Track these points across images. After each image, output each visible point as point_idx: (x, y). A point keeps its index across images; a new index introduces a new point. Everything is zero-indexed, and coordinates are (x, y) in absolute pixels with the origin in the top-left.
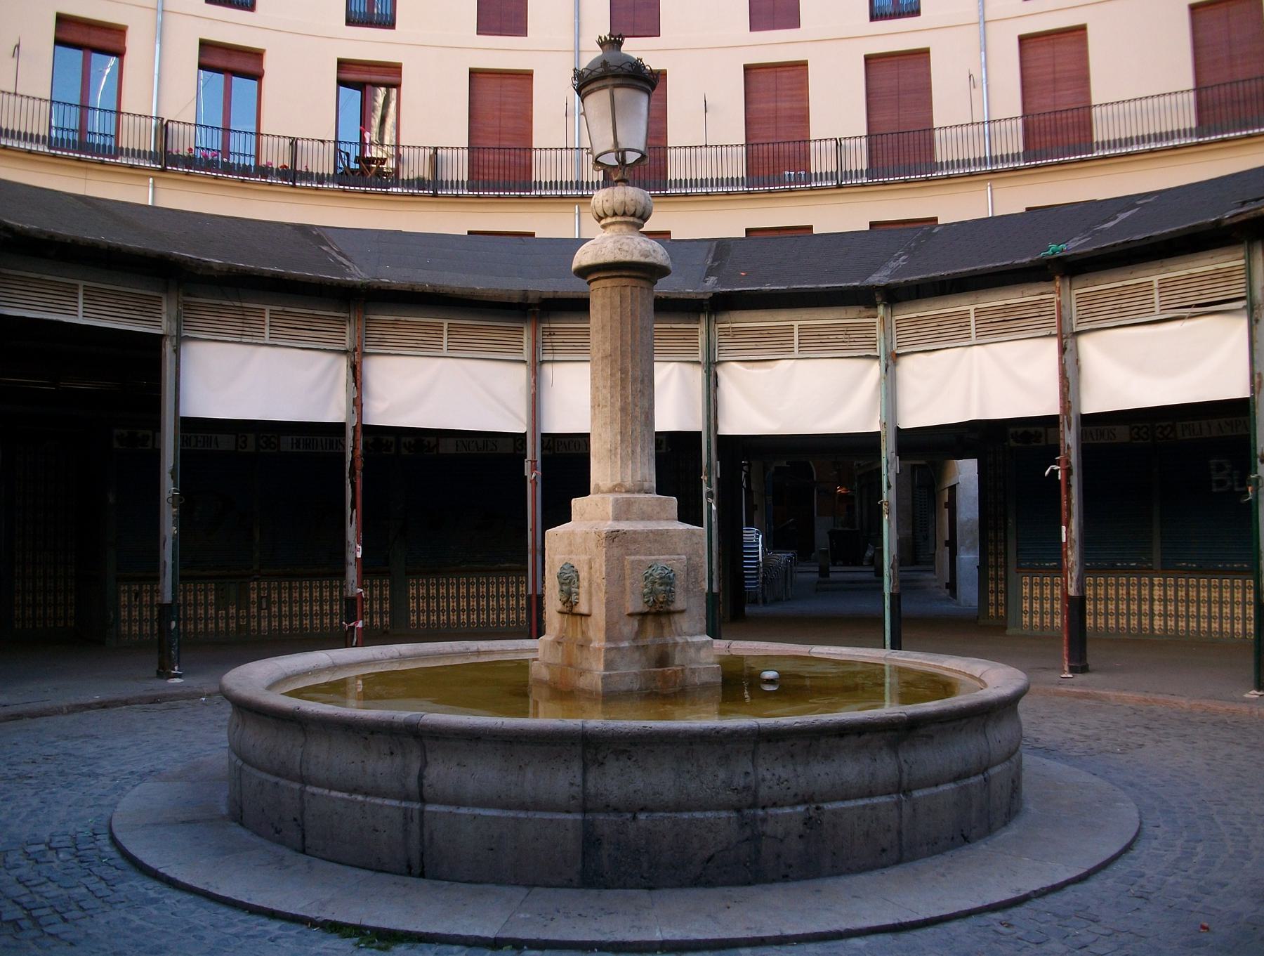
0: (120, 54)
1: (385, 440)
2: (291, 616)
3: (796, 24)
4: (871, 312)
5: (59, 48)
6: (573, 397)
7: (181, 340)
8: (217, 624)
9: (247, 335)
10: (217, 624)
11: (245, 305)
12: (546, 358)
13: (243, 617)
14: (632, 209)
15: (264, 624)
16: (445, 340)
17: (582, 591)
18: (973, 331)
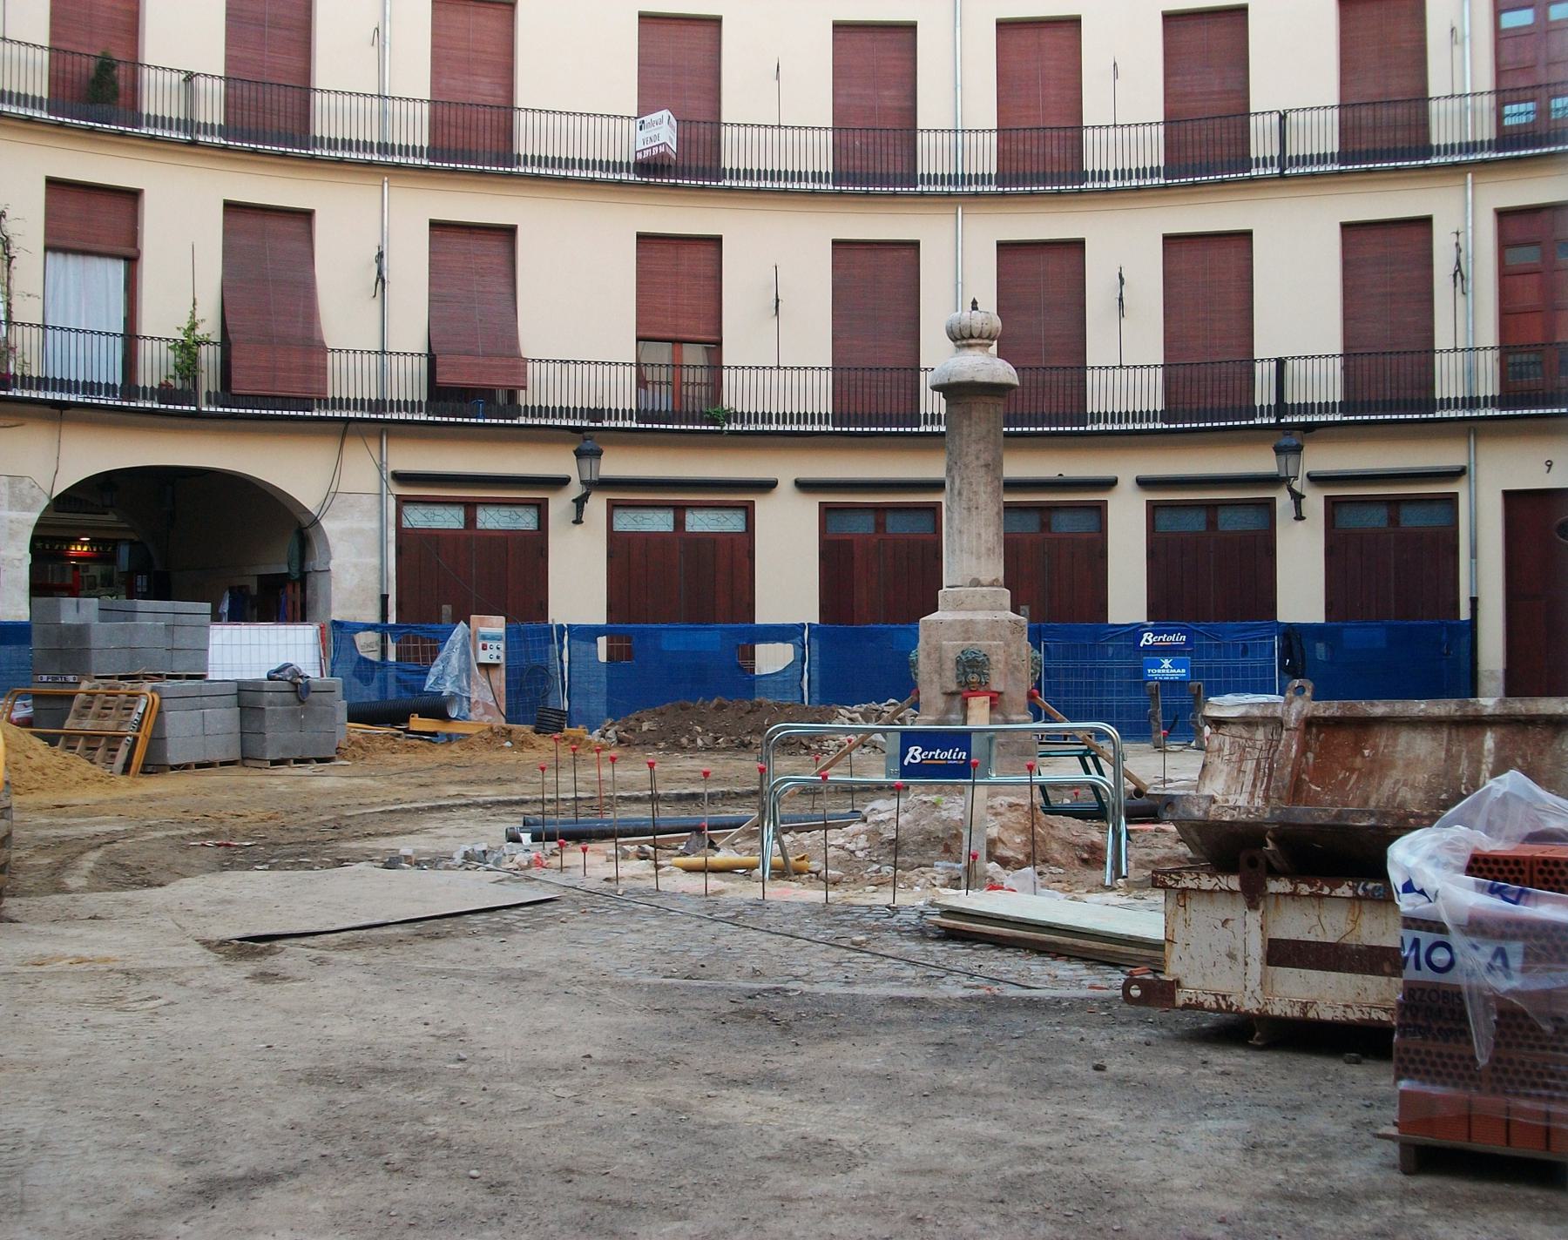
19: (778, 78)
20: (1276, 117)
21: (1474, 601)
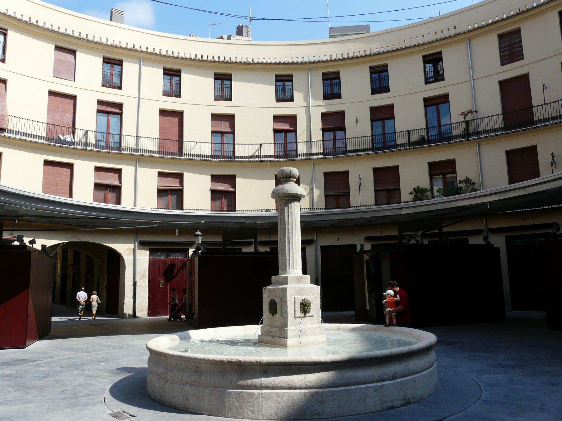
20: (407, 132)
21: (135, 284)
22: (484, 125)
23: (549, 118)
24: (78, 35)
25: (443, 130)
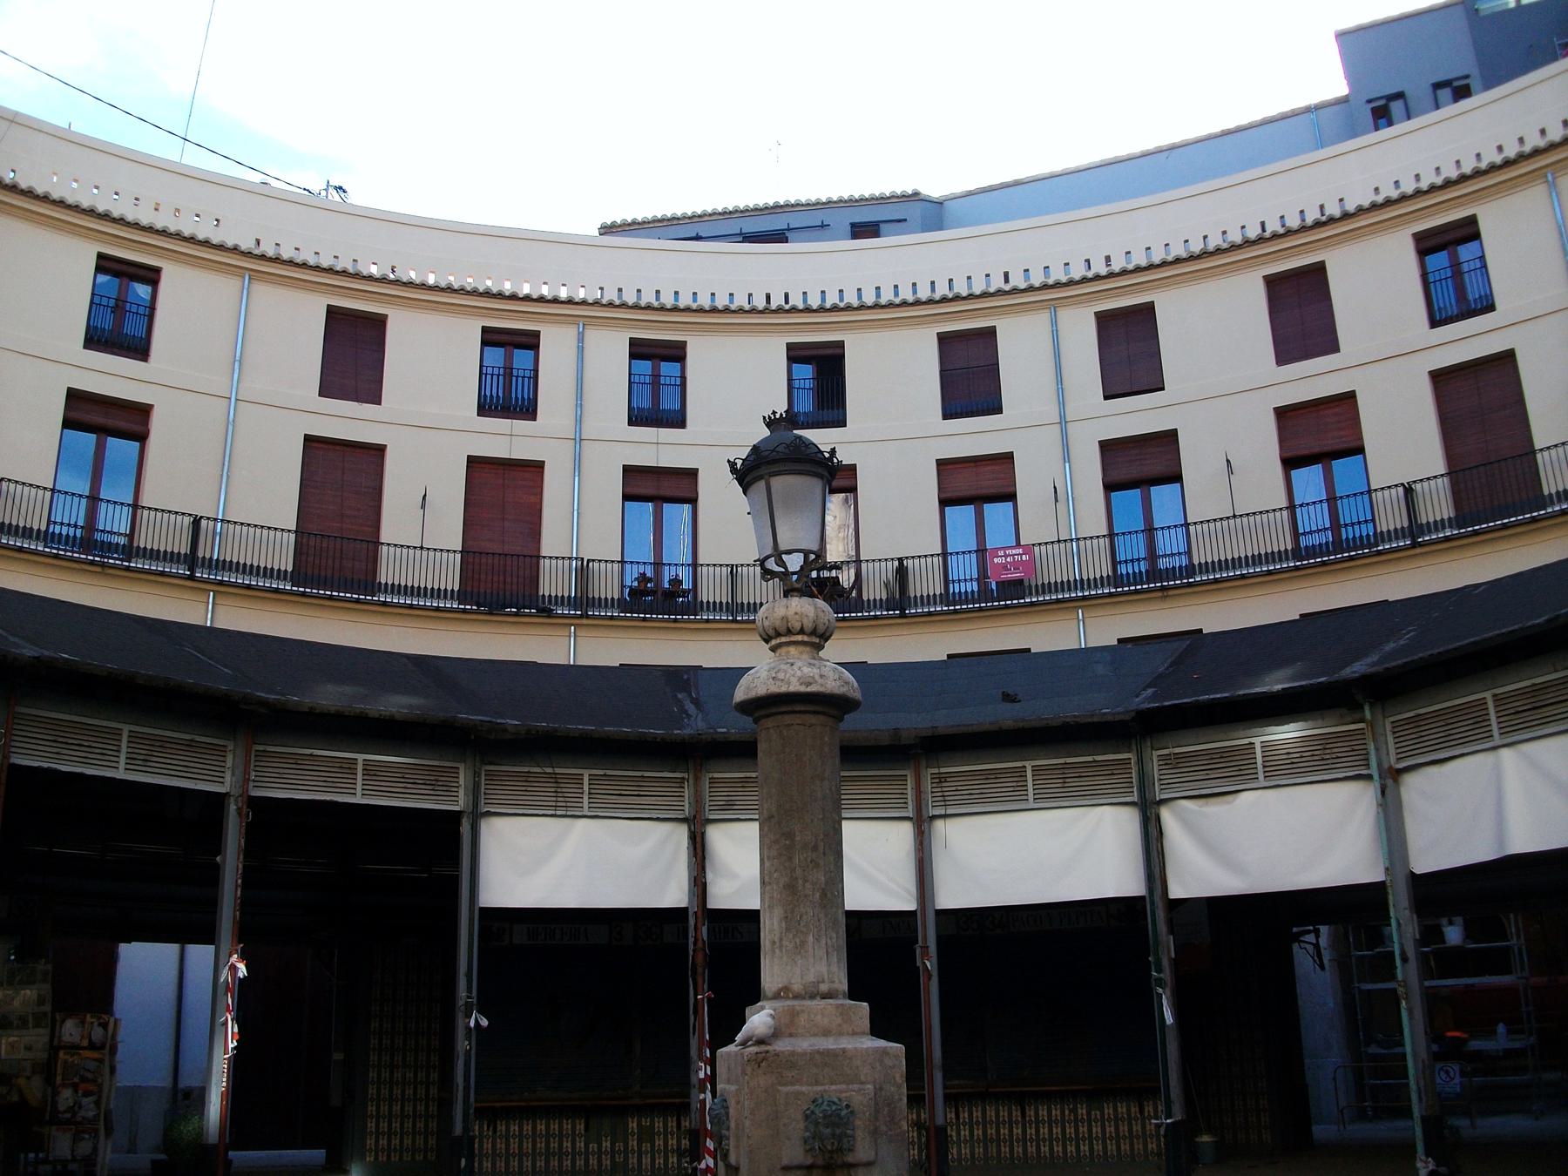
0: (693, 501)
1: (1442, 892)
2: (1118, 1138)
3: (1334, 348)
4: (1357, 716)
5: (632, 506)
6: (739, 866)
7: (477, 816)
8: (587, 1161)
9: (563, 807)
10: (587, 1161)
11: (558, 770)
12: (937, 812)
13: (619, 1152)
14: (797, 626)
15: (646, 1161)
16: (1493, 716)
17: (731, 1134)
18: (1495, 727)
19: (423, 506)
20: (1401, 489)
22: (1057, 569)
23: (1558, 492)
24: (1259, 231)
25: (1347, 513)
